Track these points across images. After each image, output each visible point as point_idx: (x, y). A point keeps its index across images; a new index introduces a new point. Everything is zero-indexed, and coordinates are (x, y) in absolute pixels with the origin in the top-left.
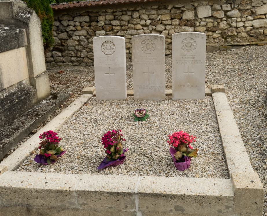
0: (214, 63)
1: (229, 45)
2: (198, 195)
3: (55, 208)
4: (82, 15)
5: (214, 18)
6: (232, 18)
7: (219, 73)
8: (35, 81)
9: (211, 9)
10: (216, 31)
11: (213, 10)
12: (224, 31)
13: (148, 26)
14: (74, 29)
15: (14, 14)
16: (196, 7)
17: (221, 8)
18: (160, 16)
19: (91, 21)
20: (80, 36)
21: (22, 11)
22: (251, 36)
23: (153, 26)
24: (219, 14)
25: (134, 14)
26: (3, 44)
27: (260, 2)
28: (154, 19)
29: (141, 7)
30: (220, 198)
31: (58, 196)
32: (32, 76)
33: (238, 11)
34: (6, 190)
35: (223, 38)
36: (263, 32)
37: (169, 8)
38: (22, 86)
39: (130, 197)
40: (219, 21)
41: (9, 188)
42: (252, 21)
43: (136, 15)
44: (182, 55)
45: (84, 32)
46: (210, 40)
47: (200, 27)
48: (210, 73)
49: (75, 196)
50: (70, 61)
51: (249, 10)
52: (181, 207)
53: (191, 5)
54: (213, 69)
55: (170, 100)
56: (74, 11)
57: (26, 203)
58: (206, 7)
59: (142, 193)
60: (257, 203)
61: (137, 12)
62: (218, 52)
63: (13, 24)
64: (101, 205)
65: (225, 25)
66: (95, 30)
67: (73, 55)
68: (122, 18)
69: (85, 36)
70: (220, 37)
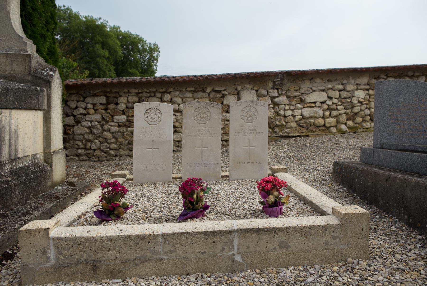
1: (277, 136)
3: (132, 261)
4: (97, 94)
6: (280, 105)
8: (52, 158)
9: (257, 95)
12: (271, 120)
14: (85, 112)
15: (32, 70)
16: (239, 91)
17: (268, 94)
19: (108, 103)
20: (93, 121)
21: (41, 67)
22: (301, 126)
25: (164, 97)
27: (309, 89)
30: (327, 226)
31: (138, 244)
32: (49, 150)
33: (285, 98)
34: (67, 242)
36: (314, 123)
37: (208, 91)
38: (36, 161)
39: (228, 236)
41: (72, 239)
42: (301, 109)
44: (241, 126)
45: (98, 117)
49: (160, 241)
50: (75, 155)
51: (298, 97)
52: (286, 243)
53: (234, 89)
57: (93, 258)
58: (251, 92)
59: (243, 229)
60: (364, 229)
61: (168, 95)
64: (192, 251)
65: (272, 114)
66: (112, 115)
67: (80, 146)
69: (99, 122)
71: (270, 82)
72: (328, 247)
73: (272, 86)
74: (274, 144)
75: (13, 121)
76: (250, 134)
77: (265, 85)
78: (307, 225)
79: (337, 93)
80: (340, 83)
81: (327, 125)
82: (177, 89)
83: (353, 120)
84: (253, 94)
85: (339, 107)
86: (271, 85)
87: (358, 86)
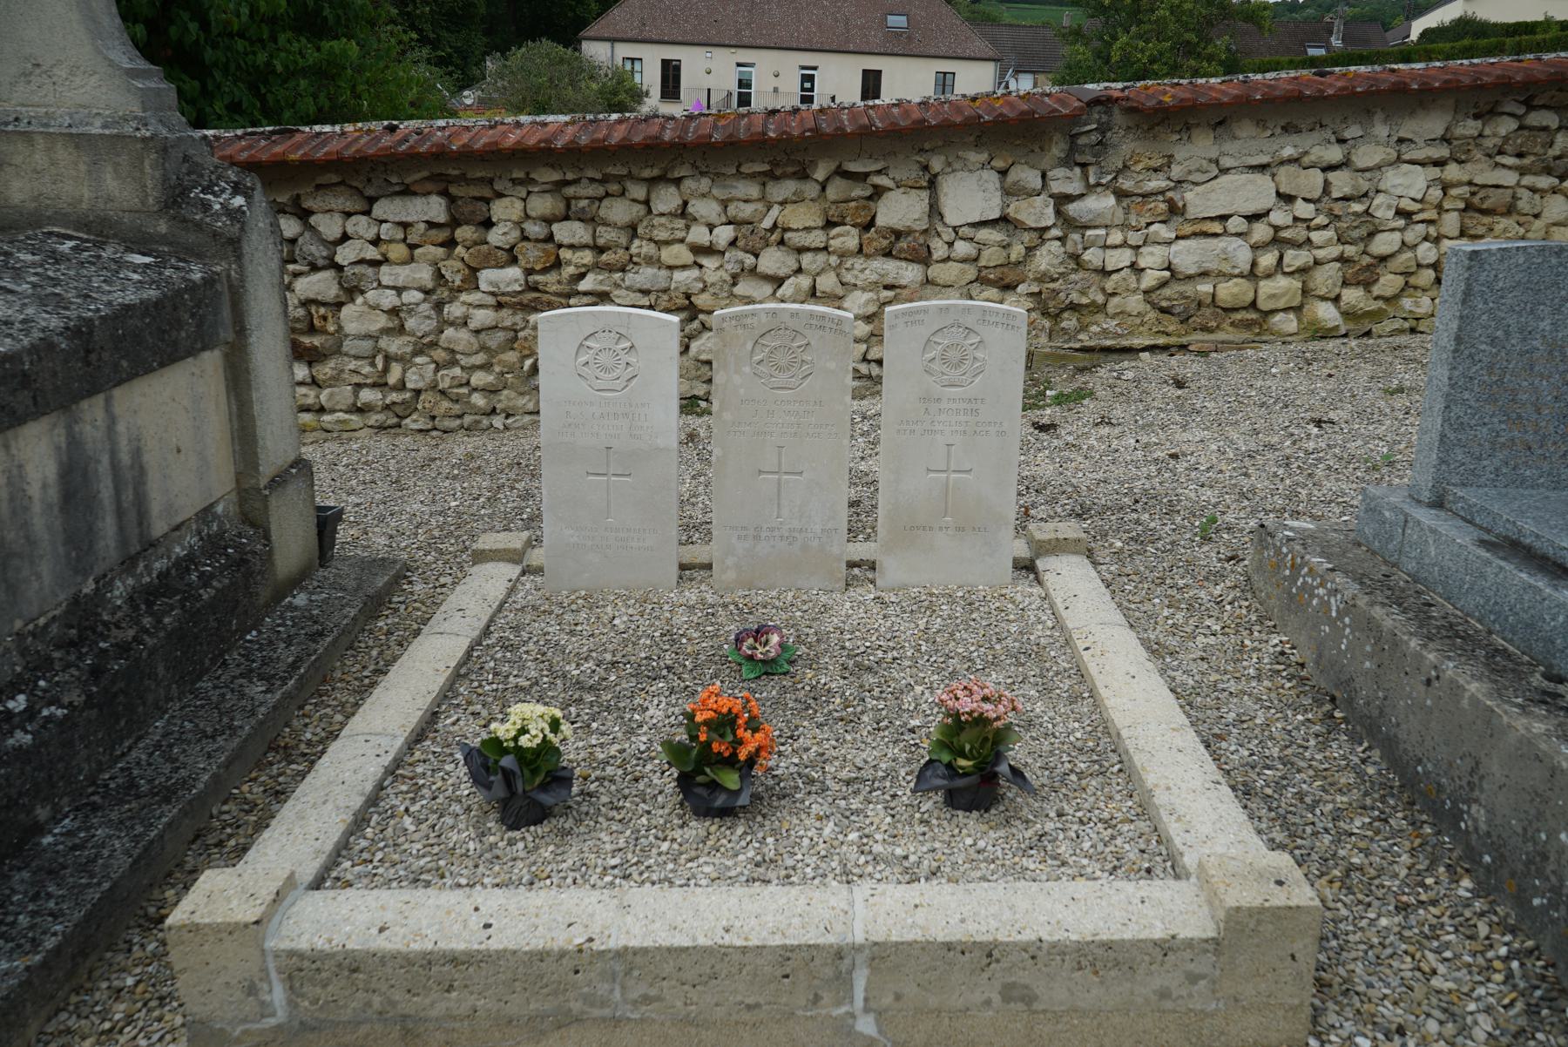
2: (1089, 939)
11: (1009, 192)
13: (723, 253)
14: (372, 253)
17: (1044, 184)
18: (775, 210)
19: (454, 223)
26: (148, 337)
27: (1205, 163)
29: (694, 166)
32: (253, 481)
33: (1112, 200)
37: (820, 175)
43: (667, 200)
47: (950, 263)
52: (1026, 987)
53: (916, 167)
56: (373, 170)
60: (1297, 955)
63: (163, 239)
65: (1056, 262)
68: (602, 213)
72: (1168, 1005)
75: (121, 427)
76: (954, 428)
78: (1104, 937)
79: (1317, 177)
80: (1333, 139)
81: (1264, 305)
83: (1367, 285)
85: (1315, 235)
86: (1057, 150)
87: (1404, 148)
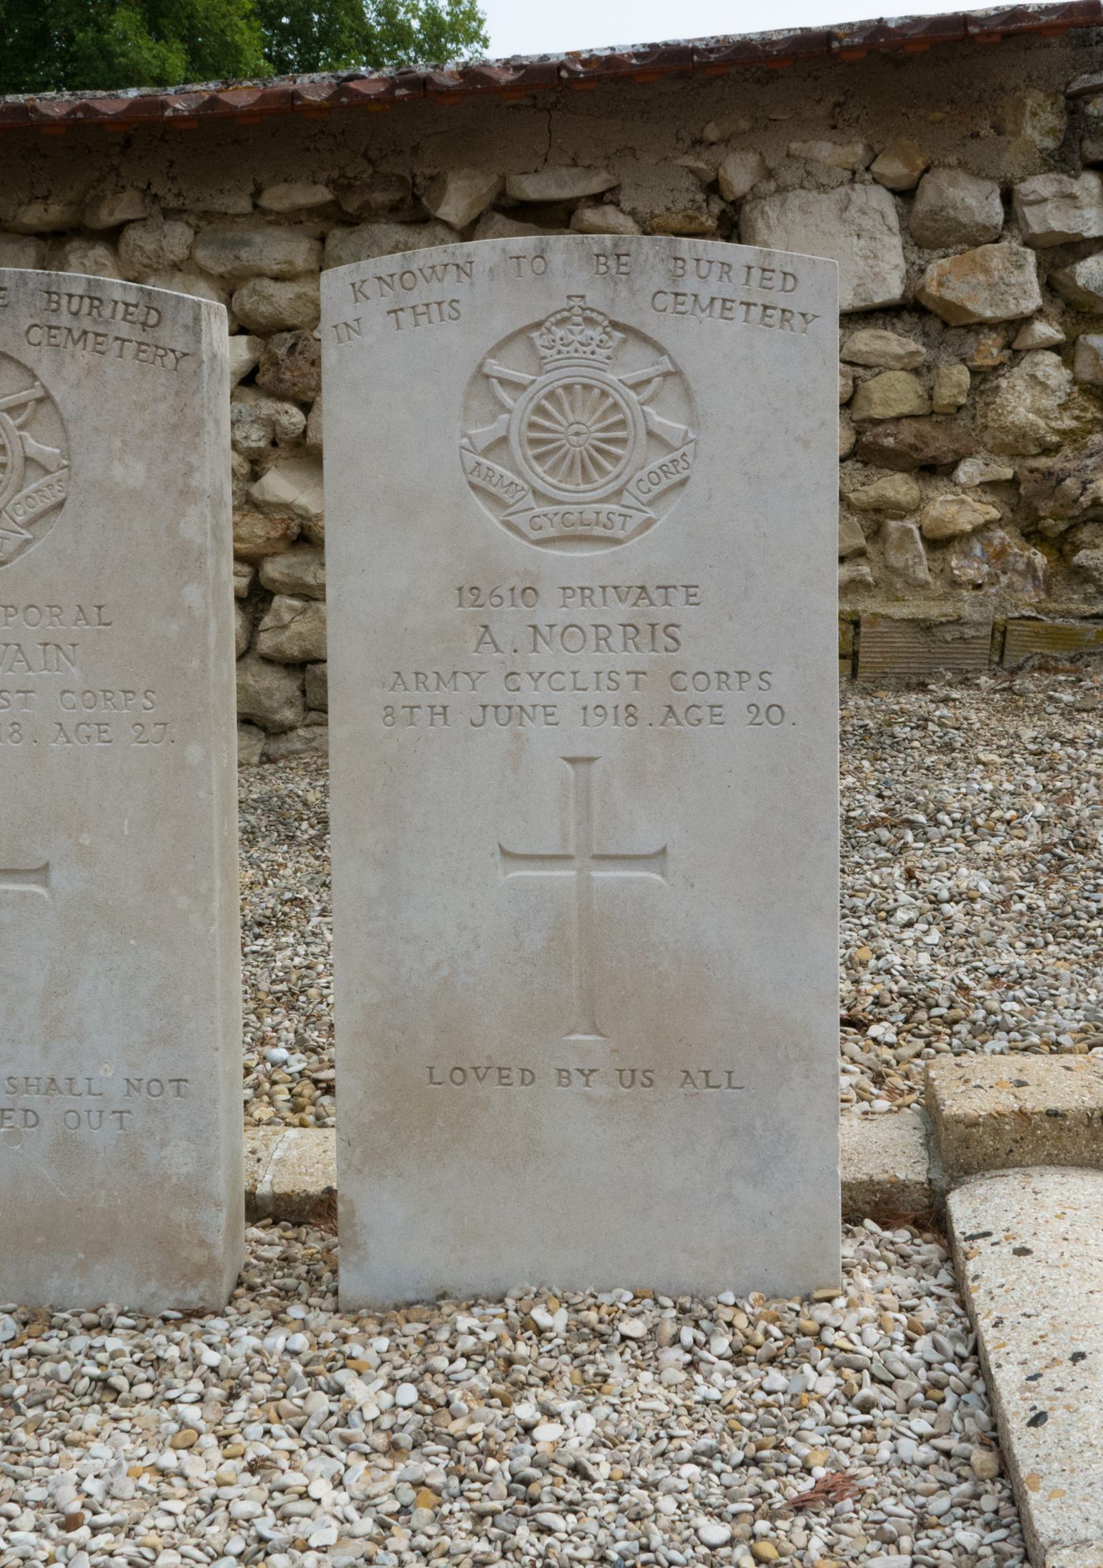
0: (948, 790)
5: (934, 326)
7: (1020, 906)
9: (905, 230)
10: (954, 466)
12: (1043, 463)
16: (737, 205)
17: (1011, 217)
23: (282, 398)
24: (982, 278)
28: (289, 329)
35: (1033, 535)
40: (990, 349)
44: (469, 593)
46: (896, 559)
48: (906, 904)
53: (687, 182)
54: (942, 860)
55: (296, 1311)
62: (984, 680)
65: (1050, 403)
70: (1000, 523)
71: (1033, 99)
73: (1050, 143)
74: (1067, 697)
76: (592, 698)
77: (986, 130)
82: (173, 203)
84: (867, 223)
